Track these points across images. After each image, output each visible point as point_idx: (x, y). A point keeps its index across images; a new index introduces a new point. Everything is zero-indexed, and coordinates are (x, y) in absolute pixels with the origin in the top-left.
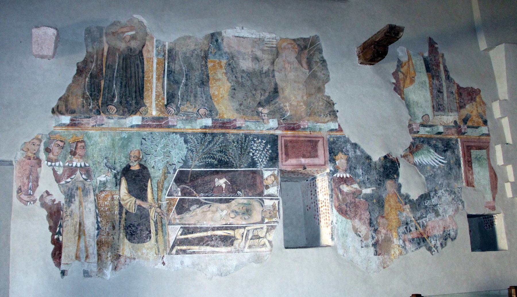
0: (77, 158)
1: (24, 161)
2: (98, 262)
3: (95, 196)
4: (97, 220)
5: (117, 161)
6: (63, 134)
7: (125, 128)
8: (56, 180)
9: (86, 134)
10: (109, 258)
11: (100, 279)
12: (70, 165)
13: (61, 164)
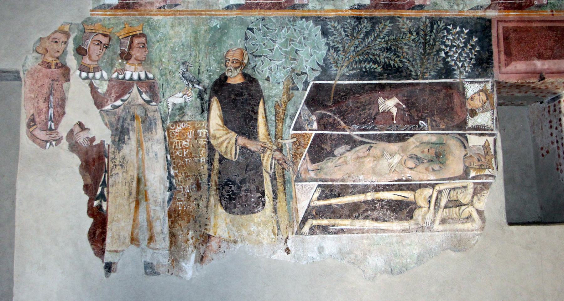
0: (133, 64)
1: (40, 71)
2: (170, 247)
3: (164, 130)
5: (202, 69)
6: (107, 23)
7: (216, 11)
8: (96, 104)
9: (148, 22)
10: (191, 241)
11: (174, 278)
12: (121, 77)
13: (105, 75)
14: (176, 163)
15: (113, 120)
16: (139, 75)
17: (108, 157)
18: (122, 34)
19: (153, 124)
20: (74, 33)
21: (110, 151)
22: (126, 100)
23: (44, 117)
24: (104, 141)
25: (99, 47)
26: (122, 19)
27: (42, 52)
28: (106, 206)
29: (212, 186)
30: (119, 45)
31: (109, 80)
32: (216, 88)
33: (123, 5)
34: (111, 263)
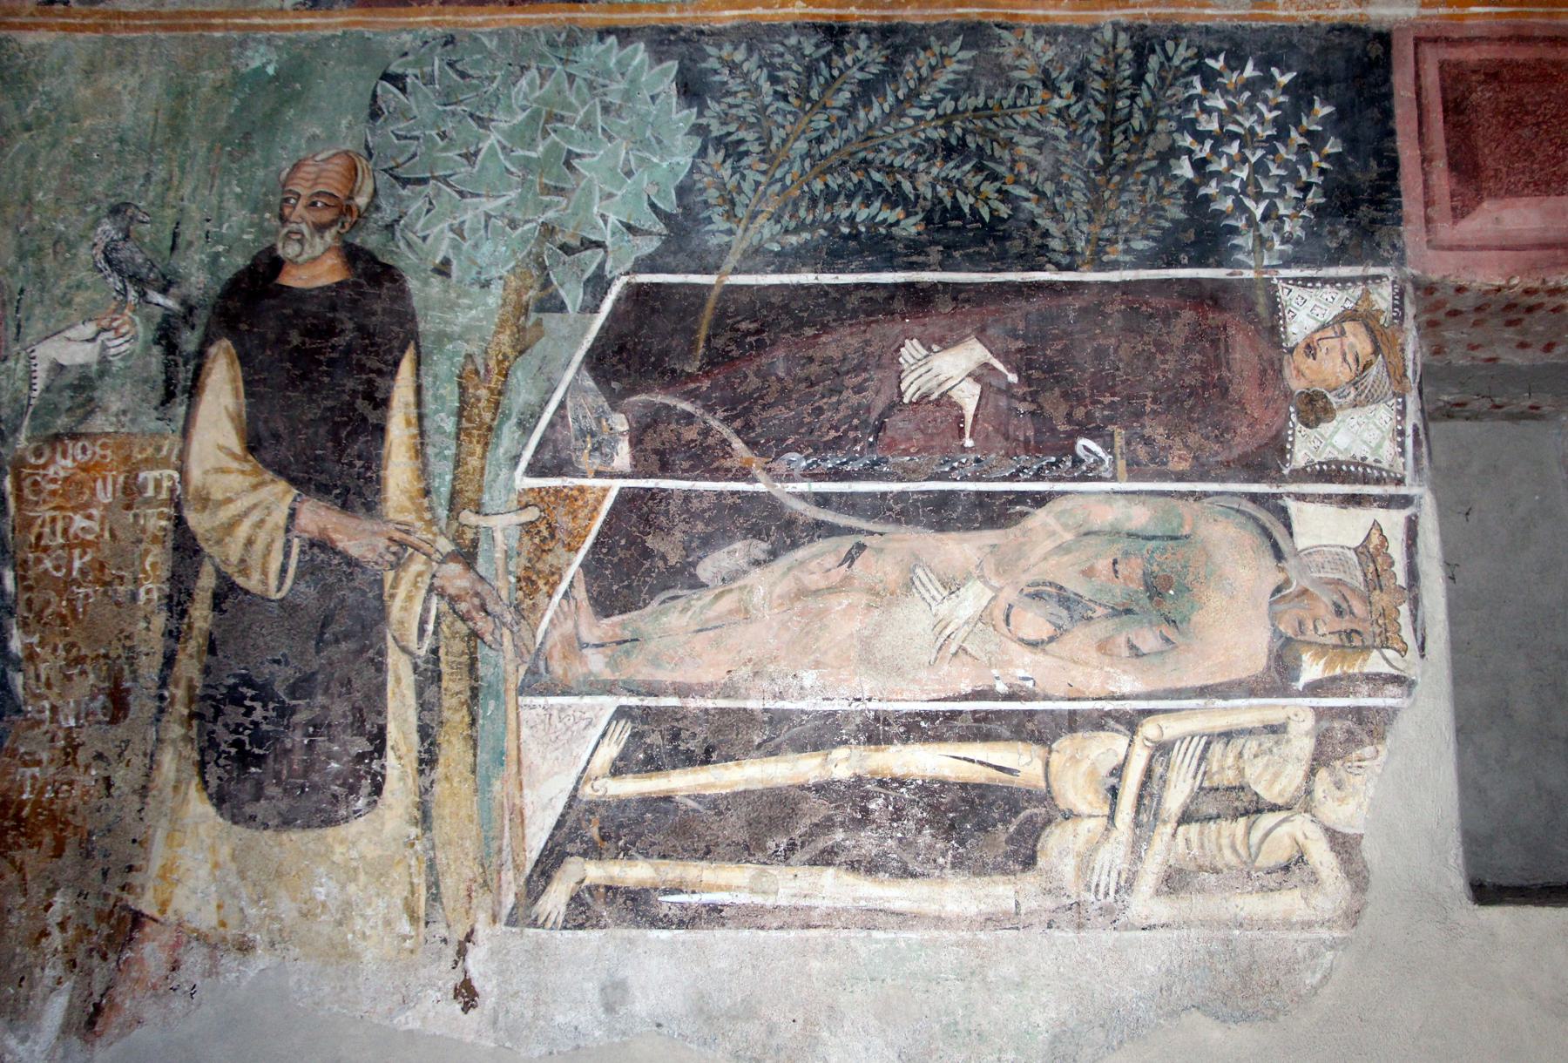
5: (188, 233)
10: (56, 940)
14: (36, 606)
29: (172, 703)
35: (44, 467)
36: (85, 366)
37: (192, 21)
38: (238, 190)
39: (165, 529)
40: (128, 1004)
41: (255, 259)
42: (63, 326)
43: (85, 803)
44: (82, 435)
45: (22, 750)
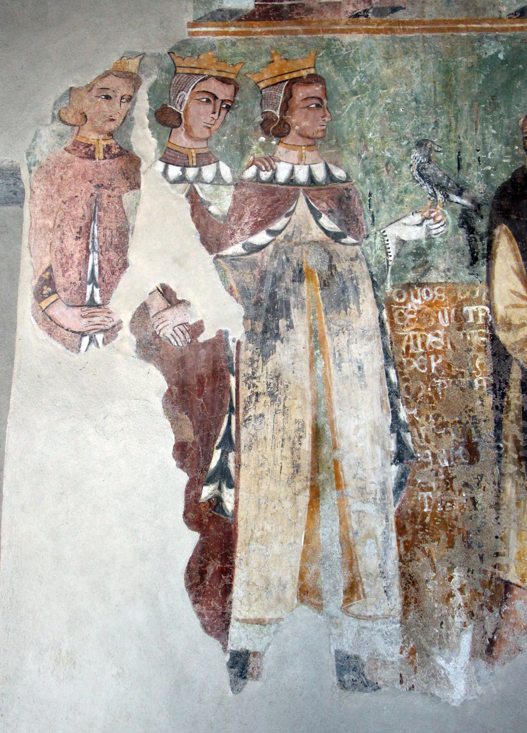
0: (295, 147)
1: (67, 165)
2: (405, 613)
3: (379, 305)
4: (395, 414)
5: (467, 159)
6: (228, 52)
7: (494, 20)
8: (204, 241)
9: (328, 47)
10: (459, 599)
11: (417, 701)
12: (265, 175)
13: (226, 172)
14: (413, 390)
15: (249, 279)
16: (310, 170)
17: (237, 374)
18: (266, 76)
19: (351, 290)
20: (149, 75)
21: (242, 357)
22: (279, 232)
23: (76, 275)
24: (226, 333)
25: (210, 108)
26: (264, 43)
27: (73, 121)
28: (232, 499)
29: (506, 451)
30: (258, 103)
31: (236, 185)
32: (506, 203)
33: (267, 11)
34: (247, 653)
35: (405, 304)
36: (418, 241)
37: (442, 26)
38: (494, 131)
39: (485, 343)
40: (511, 638)
41: (513, 174)
42: (400, 216)
43: (462, 514)
44: (424, 284)
45: (419, 481)
